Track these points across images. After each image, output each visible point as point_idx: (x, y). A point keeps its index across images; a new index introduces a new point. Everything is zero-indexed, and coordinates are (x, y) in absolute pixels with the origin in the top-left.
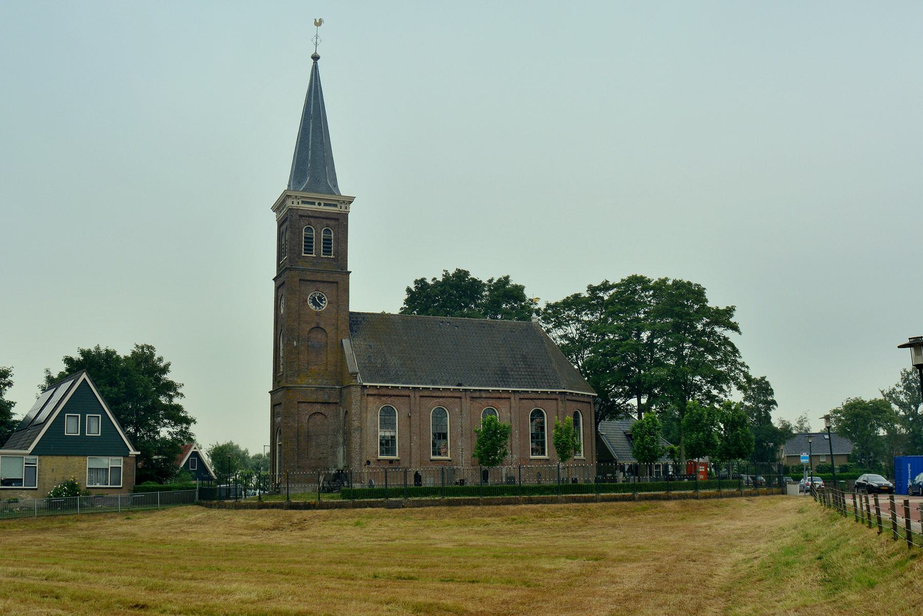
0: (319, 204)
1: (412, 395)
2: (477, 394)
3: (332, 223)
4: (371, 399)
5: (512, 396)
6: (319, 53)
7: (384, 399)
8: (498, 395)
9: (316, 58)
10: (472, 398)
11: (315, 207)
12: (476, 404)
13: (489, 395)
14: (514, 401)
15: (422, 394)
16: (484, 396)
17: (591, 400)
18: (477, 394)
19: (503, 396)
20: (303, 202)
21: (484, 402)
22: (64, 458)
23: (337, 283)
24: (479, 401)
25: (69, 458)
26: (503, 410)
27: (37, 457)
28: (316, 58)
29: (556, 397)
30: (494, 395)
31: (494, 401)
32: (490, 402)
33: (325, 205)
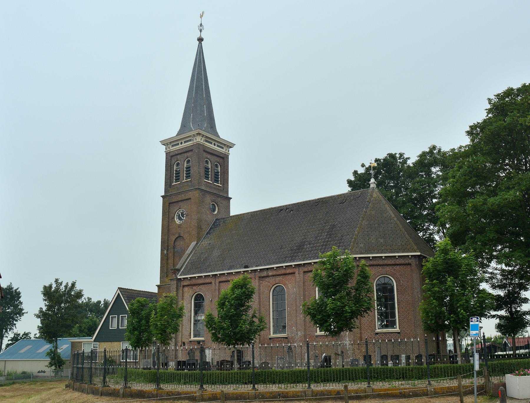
0: (215, 145)
1: (213, 282)
2: (265, 274)
3: (189, 154)
4: (186, 289)
5: (296, 271)
6: (202, 36)
7: (194, 288)
8: (283, 271)
9: (200, 40)
10: (261, 278)
11: (212, 146)
12: (265, 283)
13: (274, 273)
14: (299, 275)
15: (221, 280)
16: (270, 274)
17: (413, 262)
18: (265, 274)
19: (288, 271)
20: (173, 146)
21: (272, 280)
22: (110, 343)
23: (190, 199)
24: (267, 279)
25: (113, 343)
26: (290, 286)
27: (98, 343)
28: (200, 40)
29: (410, 261)
30: (280, 272)
31: (280, 278)
32: (278, 279)
33: (185, 142)
